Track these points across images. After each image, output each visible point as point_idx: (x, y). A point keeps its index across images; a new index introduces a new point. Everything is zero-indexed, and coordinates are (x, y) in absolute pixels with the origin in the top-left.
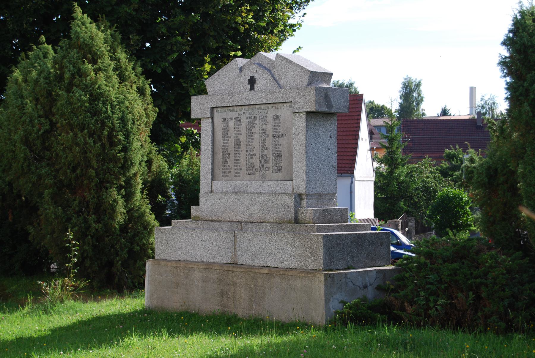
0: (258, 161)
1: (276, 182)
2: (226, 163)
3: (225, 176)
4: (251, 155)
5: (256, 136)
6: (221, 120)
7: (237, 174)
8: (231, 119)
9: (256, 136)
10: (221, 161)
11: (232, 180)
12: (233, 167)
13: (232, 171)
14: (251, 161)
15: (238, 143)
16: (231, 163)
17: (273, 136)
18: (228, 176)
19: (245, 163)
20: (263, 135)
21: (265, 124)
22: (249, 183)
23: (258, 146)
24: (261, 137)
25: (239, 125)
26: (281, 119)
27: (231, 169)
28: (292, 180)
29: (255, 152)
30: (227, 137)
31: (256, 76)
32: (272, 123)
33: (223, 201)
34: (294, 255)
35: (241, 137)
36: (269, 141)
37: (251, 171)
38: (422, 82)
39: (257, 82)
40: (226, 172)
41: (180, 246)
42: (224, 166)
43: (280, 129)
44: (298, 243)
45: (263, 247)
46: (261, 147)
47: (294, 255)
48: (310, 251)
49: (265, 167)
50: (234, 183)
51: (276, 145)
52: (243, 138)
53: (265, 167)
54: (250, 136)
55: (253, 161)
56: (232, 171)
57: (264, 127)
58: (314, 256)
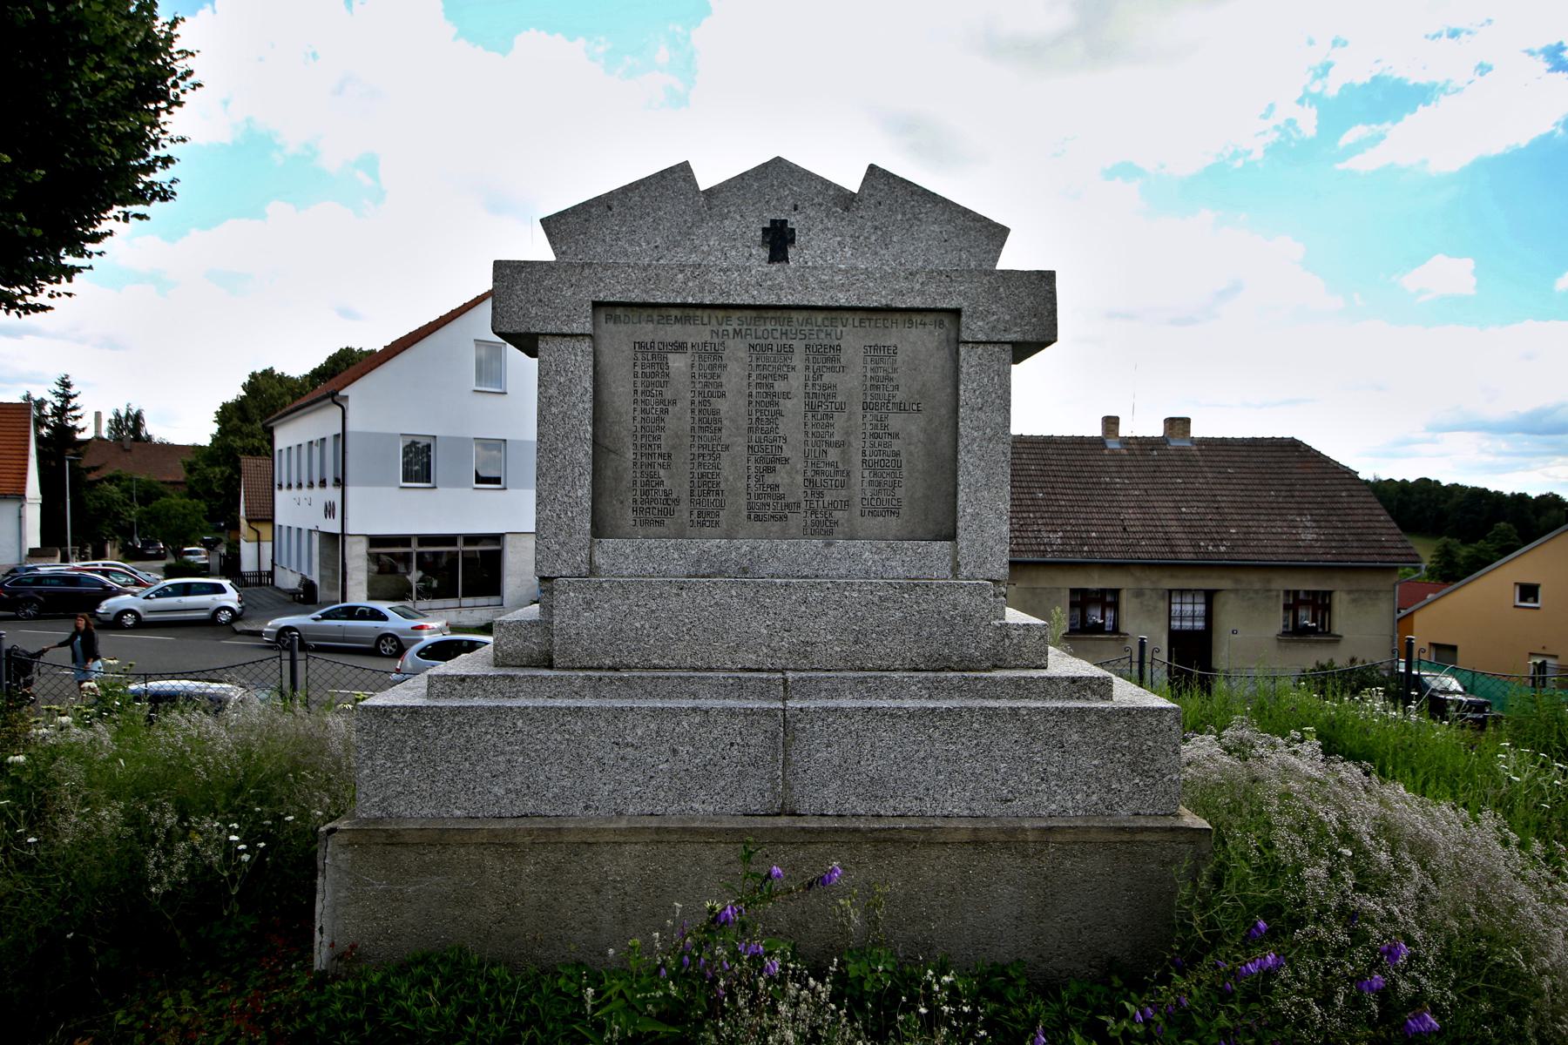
0: (800, 479)
1: (883, 544)
2: (651, 482)
3: (647, 523)
4: (769, 461)
5: (793, 408)
6: (628, 350)
7: (705, 519)
8: (680, 347)
9: (793, 408)
10: (629, 476)
11: (680, 535)
12: (685, 496)
13: (685, 506)
14: (770, 479)
15: (708, 421)
16: (675, 480)
17: (866, 407)
18: (660, 523)
19: (742, 485)
20: (820, 404)
21: (832, 369)
22: (764, 544)
23: (801, 437)
24: (812, 408)
25: (712, 367)
26: (899, 358)
27: (677, 501)
28: (952, 536)
29: (786, 453)
30: (663, 402)
31: (795, 221)
32: (859, 369)
33: (674, 604)
34: (1058, 775)
35: (723, 406)
36: (851, 424)
37: (768, 510)
38: (145, 415)
39: (800, 239)
40: (656, 512)
41: (502, 767)
42: (646, 493)
43: (897, 387)
44: (1075, 737)
45: (922, 754)
46: (811, 439)
47: (1058, 775)
48: (1128, 758)
49: (827, 499)
50: (694, 547)
51: (875, 436)
52: (731, 408)
53: (827, 499)
54: (766, 406)
55: (779, 480)
56: (685, 506)
57: (827, 378)
58: (1144, 774)
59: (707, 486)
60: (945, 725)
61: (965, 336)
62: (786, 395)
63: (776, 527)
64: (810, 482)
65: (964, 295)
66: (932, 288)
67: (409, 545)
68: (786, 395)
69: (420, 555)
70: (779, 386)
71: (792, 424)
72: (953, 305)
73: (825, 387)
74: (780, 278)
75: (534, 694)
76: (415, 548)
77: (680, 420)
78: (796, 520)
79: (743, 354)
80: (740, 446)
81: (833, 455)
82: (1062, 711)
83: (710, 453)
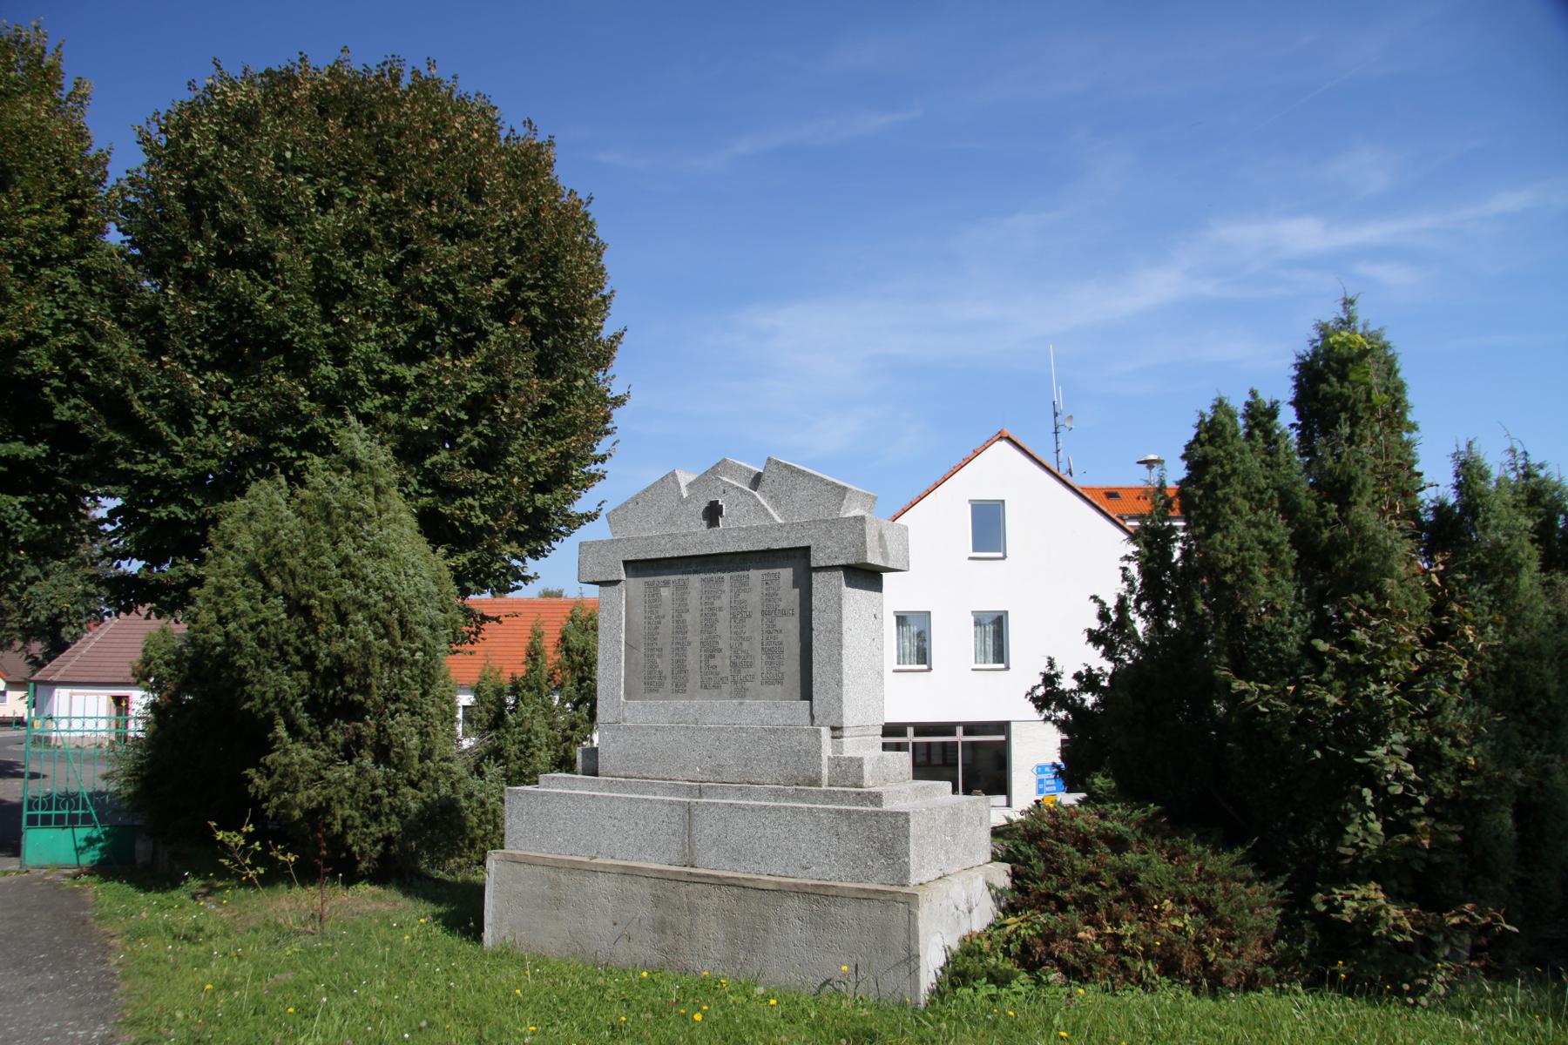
4: (711, 650)
5: (724, 616)
7: (680, 689)
9: (724, 616)
13: (669, 680)
14: (712, 662)
15: (680, 627)
17: (763, 613)
20: (739, 614)
33: (653, 739)
35: (687, 617)
37: (711, 684)
52: (692, 618)
57: (742, 596)
58: (887, 857)
59: (680, 667)
60: (773, 816)
61: (813, 564)
62: (720, 609)
63: (715, 692)
64: (734, 664)
65: (811, 537)
66: (792, 535)
67: (953, 734)
68: (720, 609)
69: (914, 744)
70: (717, 603)
71: (723, 629)
72: (805, 544)
73: (741, 602)
74: (712, 537)
75: (582, 788)
76: (910, 738)
77: (667, 627)
78: (727, 688)
79: (698, 585)
80: (696, 644)
81: (746, 644)
82: (839, 812)
83: (681, 646)
